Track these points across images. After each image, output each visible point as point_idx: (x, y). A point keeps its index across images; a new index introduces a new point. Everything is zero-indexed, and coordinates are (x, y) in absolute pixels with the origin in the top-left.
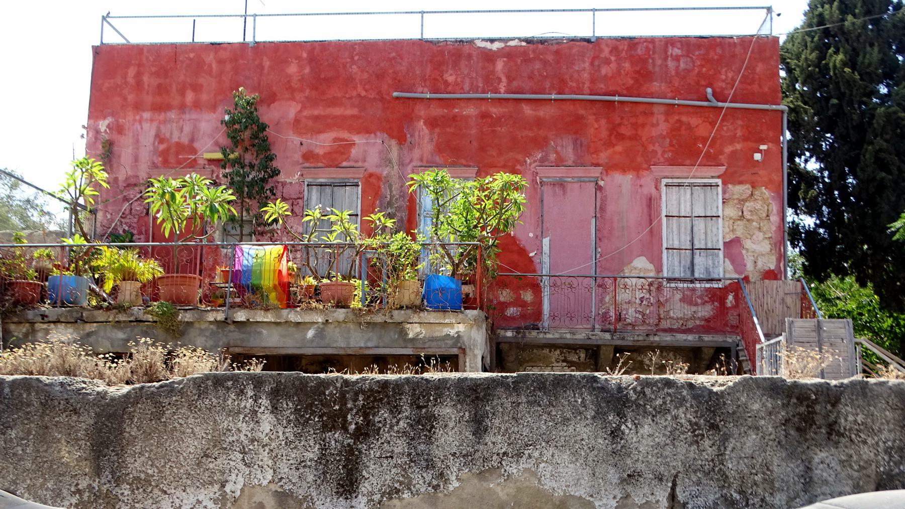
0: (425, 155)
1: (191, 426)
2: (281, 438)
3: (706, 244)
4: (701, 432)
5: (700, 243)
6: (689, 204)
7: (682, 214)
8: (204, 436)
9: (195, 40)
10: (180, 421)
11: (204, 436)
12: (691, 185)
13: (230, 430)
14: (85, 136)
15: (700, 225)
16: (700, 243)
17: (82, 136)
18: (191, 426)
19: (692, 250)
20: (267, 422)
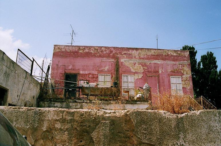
6: (175, 81)
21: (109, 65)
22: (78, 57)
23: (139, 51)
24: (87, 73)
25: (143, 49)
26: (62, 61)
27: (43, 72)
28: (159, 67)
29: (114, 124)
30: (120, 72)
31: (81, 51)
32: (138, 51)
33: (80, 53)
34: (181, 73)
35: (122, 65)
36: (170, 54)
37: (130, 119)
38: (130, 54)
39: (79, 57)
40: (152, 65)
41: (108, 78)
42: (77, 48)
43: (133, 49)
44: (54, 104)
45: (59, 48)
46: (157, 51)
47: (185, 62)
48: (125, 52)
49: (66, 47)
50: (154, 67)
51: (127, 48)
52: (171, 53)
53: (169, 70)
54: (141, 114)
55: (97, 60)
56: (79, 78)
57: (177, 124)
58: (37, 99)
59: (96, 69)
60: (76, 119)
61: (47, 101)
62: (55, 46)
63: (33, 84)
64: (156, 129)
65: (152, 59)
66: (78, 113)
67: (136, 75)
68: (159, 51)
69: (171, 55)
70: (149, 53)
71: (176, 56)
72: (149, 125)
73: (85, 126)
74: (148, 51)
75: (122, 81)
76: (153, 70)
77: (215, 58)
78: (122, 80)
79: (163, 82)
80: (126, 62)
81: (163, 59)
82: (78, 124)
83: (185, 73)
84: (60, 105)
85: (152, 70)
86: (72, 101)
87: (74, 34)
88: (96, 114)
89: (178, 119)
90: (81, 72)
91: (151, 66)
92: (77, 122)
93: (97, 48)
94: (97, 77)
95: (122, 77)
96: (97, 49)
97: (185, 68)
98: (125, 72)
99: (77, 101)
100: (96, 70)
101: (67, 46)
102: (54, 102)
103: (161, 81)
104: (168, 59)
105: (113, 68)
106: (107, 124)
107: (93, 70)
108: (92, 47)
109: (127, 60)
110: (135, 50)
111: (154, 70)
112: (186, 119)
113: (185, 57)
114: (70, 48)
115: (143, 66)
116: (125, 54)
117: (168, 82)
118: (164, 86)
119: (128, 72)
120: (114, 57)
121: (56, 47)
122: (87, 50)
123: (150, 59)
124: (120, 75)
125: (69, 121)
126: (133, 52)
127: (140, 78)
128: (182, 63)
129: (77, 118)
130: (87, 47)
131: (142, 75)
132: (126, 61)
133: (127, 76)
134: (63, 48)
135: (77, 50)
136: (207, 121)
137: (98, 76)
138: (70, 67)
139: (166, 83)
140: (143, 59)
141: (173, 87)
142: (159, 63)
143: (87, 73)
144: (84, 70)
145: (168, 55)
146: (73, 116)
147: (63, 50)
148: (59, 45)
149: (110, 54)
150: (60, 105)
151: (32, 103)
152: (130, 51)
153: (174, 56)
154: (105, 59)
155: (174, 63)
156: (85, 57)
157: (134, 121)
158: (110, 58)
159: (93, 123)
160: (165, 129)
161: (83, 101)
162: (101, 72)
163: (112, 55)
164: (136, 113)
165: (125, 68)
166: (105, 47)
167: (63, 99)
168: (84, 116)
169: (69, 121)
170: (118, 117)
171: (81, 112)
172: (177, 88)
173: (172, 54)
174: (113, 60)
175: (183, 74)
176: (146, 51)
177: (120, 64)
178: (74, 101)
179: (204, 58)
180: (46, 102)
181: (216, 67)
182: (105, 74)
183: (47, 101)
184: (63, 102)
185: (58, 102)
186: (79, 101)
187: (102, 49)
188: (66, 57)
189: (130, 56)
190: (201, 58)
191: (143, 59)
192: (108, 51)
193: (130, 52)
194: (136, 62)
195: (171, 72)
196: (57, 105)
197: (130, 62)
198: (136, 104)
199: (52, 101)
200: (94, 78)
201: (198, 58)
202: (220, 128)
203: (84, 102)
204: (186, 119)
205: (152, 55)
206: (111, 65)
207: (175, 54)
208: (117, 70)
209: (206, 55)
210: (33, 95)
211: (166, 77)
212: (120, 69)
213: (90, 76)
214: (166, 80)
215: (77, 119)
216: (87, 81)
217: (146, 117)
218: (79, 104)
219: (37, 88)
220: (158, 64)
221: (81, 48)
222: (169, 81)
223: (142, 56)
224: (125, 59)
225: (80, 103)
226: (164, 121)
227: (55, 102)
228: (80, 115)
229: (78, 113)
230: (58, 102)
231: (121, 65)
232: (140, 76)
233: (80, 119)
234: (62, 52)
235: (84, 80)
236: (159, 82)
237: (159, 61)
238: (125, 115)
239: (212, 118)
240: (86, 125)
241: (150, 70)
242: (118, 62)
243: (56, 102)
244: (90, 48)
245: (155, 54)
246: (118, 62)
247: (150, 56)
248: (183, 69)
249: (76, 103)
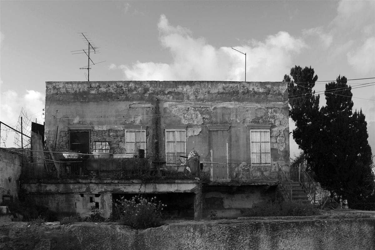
0: (138, 103)
1: (170, 243)
2: (204, 247)
3: (265, 151)
4: (348, 239)
5: (258, 145)
6: (259, 137)
7: (257, 141)
8: (176, 246)
9: (90, 81)
10: (166, 241)
11: (176, 246)
12: (261, 132)
13: (185, 244)
14: (44, 114)
15: (263, 145)
16: (258, 145)
17: (43, 114)
18: (170, 243)
19: (261, 153)
20: (198, 241)
21: (143, 114)
22: (88, 102)
23: (196, 86)
24: (105, 129)
25: (203, 82)
26: (63, 110)
27: (24, 136)
28: (230, 114)
29: (56, 242)
30: (163, 125)
31: (93, 92)
32: (194, 88)
33: (92, 94)
34: (269, 124)
35: (165, 112)
36: (251, 89)
37: (75, 236)
38: (179, 93)
39: (91, 101)
40: (219, 111)
41: (143, 137)
42: (86, 86)
43: (184, 83)
44: (46, 187)
45: (54, 88)
46: (227, 85)
47: (280, 103)
48: (170, 90)
49: (66, 85)
50: (221, 114)
51: (173, 81)
52: (253, 89)
53: (249, 119)
54: (89, 230)
55: (123, 106)
56: (93, 138)
57: (135, 242)
58: (17, 181)
59: (121, 122)
60: (11, 237)
61: (33, 183)
62: (48, 83)
63: (5, 160)
64: (108, 248)
65: (218, 100)
66: (13, 230)
67: (189, 129)
68: (231, 85)
69: (254, 92)
70: (214, 91)
71: (263, 93)
72: (99, 243)
73: (22, 245)
74: (211, 86)
75: (166, 141)
76: (220, 119)
77: (350, 88)
78: (166, 139)
79: (237, 141)
80: (173, 107)
81: (238, 100)
82: (14, 243)
83: (277, 123)
84: (54, 188)
85: (219, 121)
86: (72, 182)
87: (91, 50)
88: (35, 230)
89: (137, 236)
90: (96, 128)
91: (216, 113)
92: (12, 241)
93: (121, 84)
94: (123, 135)
95: (166, 133)
96: (122, 87)
97: (278, 114)
98: (169, 126)
99: (80, 181)
100: (121, 124)
101: (68, 83)
102: (45, 185)
103: (233, 139)
104: (247, 100)
105: (149, 119)
106: (47, 243)
107: (115, 123)
108: (111, 82)
109: (174, 103)
110: (189, 84)
111: (222, 120)
112: (148, 236)
113: (280, 94)
114: (74, 86)
115: (202, 114)
116: (170, 93)
117: (245, 140)
118: (239, 146)
119: (176, 124)
120: (151, 100)
121: (50, 87)
122: (103, 89)
123: (215, 100)
124: (162, 131)
125: (2, 240)
126: (185, 89)
127: (196, 133)
128: (272, 106)
129: (12, 235)
130: (104, 83)
131: (200, 130)
132: (172, 105)
133: (173, 132)
134: (61, 87)
135: (86, 89)
136: (176, 238)
137: (124, 134)
138: (76, 120)
139: (242, 141)
140: (202, 100)
141: (254, 148)
142: (231, 107)
143: (105, 128)
144: (100, 124)
145: (248, 92)
146: (7, 234)
147: (63, 90)
148: (55, 82)
149: (144, 93)
150: (54, 188)
151: (7, 190)
152: (180, 87)
153: (259, 94)
154: (135, 104)
155: (259, 106)
156: (101, 102)
157: (80, 239)
158: (144, 102)
159: (32, 242)
160: (120, 247)
161: (89, 181)
162: (130, 126)
163: (148, 95)
164: (83, 229)
165: (169, 119)
166: (135, 82)
167: (58, 179)
168: (20, 234)
169: (2, 240)
170: (60, 235)
171: (16, 229)
172: (260, 150)
173: (256, 89)
174: (149, 105)
175: (273, 126)
176: (207, 86)
177: (161, 110)
178: (75, 181)
179: (330, 87)
180: (32, 185)
181: (352, 105)
182: (137, 130)
183: (34, 182)
184: (59, 183)
185: (50, 183)
186: (84, 181)
187: (130, 85)
188: (69, 103)
189: (179, 97)
190: (325, 88)
191: (202, 100)
192: (140, 89)
193: (180, 89)
194: (189, 107)
195: (251, 122)
196: (50, 188)
197: (180, 106)
198: (174, 183)
199: (41, 183)
200: (117, 136)
201: (319, 89)
202: (192, 246)
203: (91, 183)
204: (148, 236)
205: (218, 93)
206: (147, 114)
207: (261, 90)
208: (157, 122)
209: (334, 83)
210: (7, 177)
211: (242, 130)
212: (162, 120)
213: (111, 134)
214: (242, 136)
215: (12, 237)
216: (106, 142)
217: (95, 234)
218: (84, 186)
219: (15, 164)
220: (230, 109)
221: (93, 85)
222: (247, 139)
223: (201, 96)
224: (171, 103)
225: (85, 184)
226: (119, 238)
227: (47, 183)
228: (16, 233)
229: (13, 230)
230: (52, 184)
231: (163, 113)
232: (197, 131)
233: (16, 237)
234: (61, 94)
235: (102, 142)
236: (230, 141)
237: (231, 104)
238: (69, 232)
239: (184, 235)
240: (23, 244)
241: (214, 119)
242: (159, 108)
243: (48, 183)
244: (108, 84)
245: (225, 92)
246: (157, 111)
247: (214, 96)
248: (273, 117)
249: (80, 185)
